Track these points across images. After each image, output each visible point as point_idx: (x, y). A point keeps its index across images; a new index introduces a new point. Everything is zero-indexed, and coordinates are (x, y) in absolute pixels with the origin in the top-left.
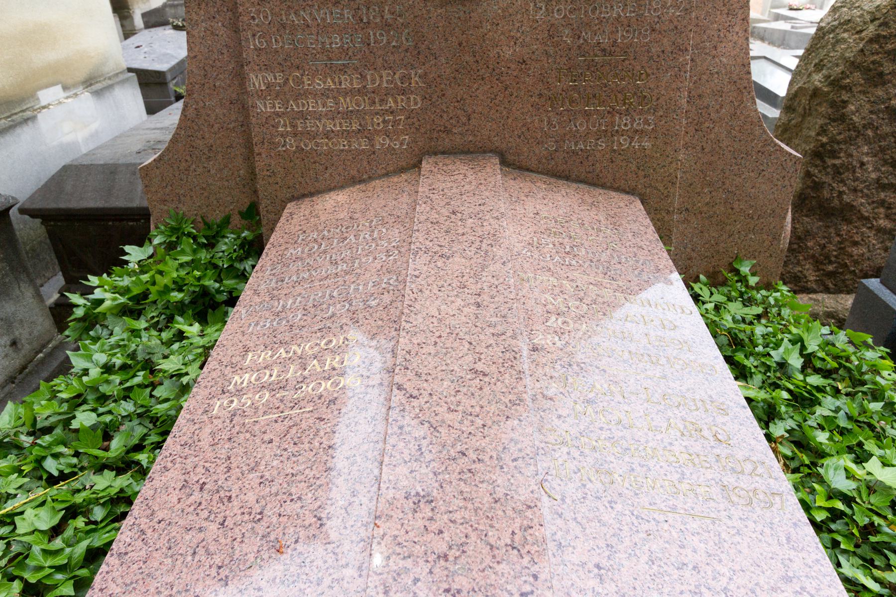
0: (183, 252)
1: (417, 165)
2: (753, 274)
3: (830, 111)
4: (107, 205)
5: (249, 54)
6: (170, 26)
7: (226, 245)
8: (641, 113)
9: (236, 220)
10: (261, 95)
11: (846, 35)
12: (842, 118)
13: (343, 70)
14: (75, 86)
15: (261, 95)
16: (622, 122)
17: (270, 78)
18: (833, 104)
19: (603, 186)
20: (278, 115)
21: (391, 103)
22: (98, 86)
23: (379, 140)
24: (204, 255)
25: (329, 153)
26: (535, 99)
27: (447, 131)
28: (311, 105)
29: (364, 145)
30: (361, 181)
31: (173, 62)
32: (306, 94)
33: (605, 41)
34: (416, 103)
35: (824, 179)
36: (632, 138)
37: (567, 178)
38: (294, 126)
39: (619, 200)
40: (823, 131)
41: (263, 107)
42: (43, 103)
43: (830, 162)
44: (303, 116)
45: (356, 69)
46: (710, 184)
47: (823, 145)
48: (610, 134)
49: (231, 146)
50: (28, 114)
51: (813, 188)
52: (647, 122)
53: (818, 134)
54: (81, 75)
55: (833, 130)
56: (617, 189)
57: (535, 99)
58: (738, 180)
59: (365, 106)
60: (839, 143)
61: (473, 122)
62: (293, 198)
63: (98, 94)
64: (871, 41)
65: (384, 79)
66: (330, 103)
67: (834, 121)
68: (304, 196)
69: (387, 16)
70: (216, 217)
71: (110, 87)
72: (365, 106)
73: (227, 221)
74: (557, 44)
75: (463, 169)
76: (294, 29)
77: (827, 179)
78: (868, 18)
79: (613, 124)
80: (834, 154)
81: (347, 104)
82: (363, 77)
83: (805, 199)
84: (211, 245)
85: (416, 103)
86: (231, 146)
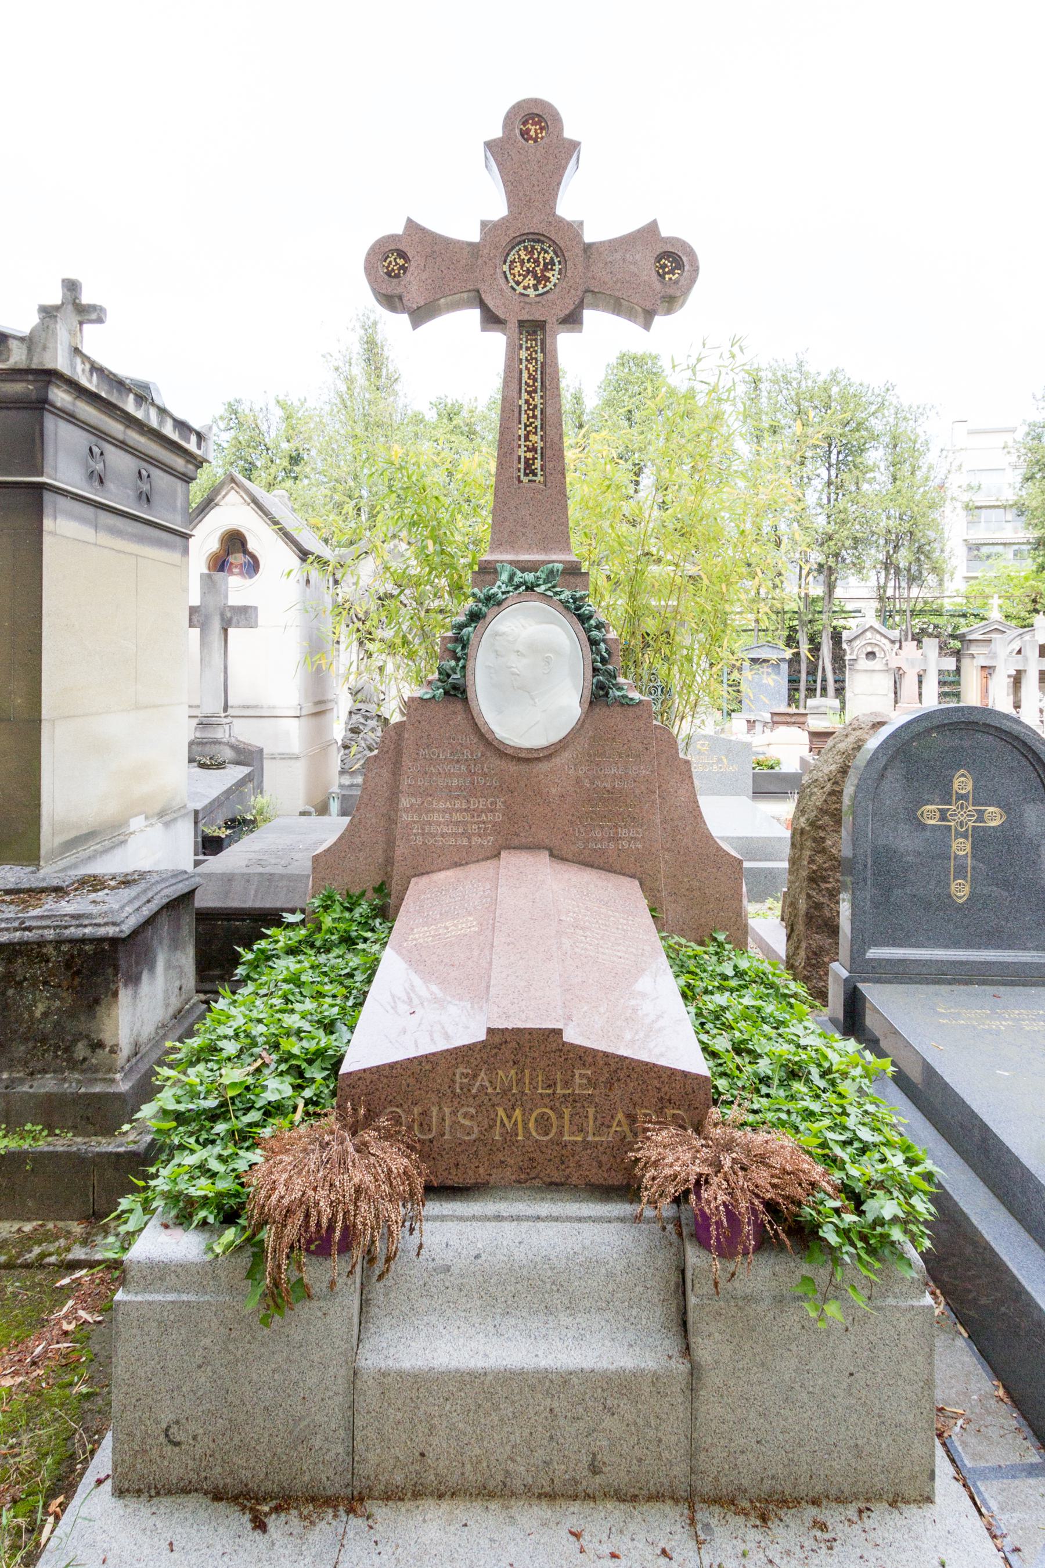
0: (335, 911)
1: (498, 855)
2: (729, 943)
3: (814, 845)
4: (224, 905)
5: (404, 787)
6: (195, 764)
7: (363, 908)
8: (634, 826)
9: (370, 894)
10: (406, 810)
11: (815, 790)
12: (823, 851)
13: (457, 797)
14: (152, 817)
15: (406, 810)
16: (622, 832)
17: (413, 800)
18: (814, 840)
19: (615, 872)
20: (414, 822)
21: (484, 817)
22: (167, 818)
23: (475, 839)
24: (347, 915)
25: (442, 848)
26: (570, 817)
27: (518, 835)
28: (436, 817)
29: (465, 842)
30: (461, 865)
31: (207, 801)
32: (433, 811)
33: (609, 786)
34: (499, 817)
35: (822, 900)
36: (630, 842)
37: (592, 866)
38: (423, 829)
39: (626, 881)
40: (812, 861)
41: (406, 817)
42: (131, 830)
43: (823, 886)
44: (430, 823)
45: (465, 797)
46: (687, 876)
47: (814, 872)
48: (616, 839)
49: (376, 843)
50: (121, 838)
51: (815, 908)
52: (637, 832)
53: (809, 863)
54: (157, 807)
55: (819, 859)
56: (624, 875)
57: (570, 817)
58: (705, 874)
59: (468, 818)
60: (826, 870)
61: (533, 830)
62: (415, 875)
63: (167, 824)
64: (830, 794)
65: (479, 803)
66: (447, 816)
67: (819, 852)
68: (423, 874)
69: (485, 770)
70: (356, 891)
71: (175, 820)
72: (468, 818)
73: (363, 894)
74: (581, 787)
75: (526, 856)
76: (432, 774)
77: (825, 900)
78: (826, 778)
79: (617, 833)
80: (825, 879)
81: (457, 817)
82: (468, 802)
83: (812, 917)
84: (350, 910)
85: (499, 817)
86: (376, 843)
